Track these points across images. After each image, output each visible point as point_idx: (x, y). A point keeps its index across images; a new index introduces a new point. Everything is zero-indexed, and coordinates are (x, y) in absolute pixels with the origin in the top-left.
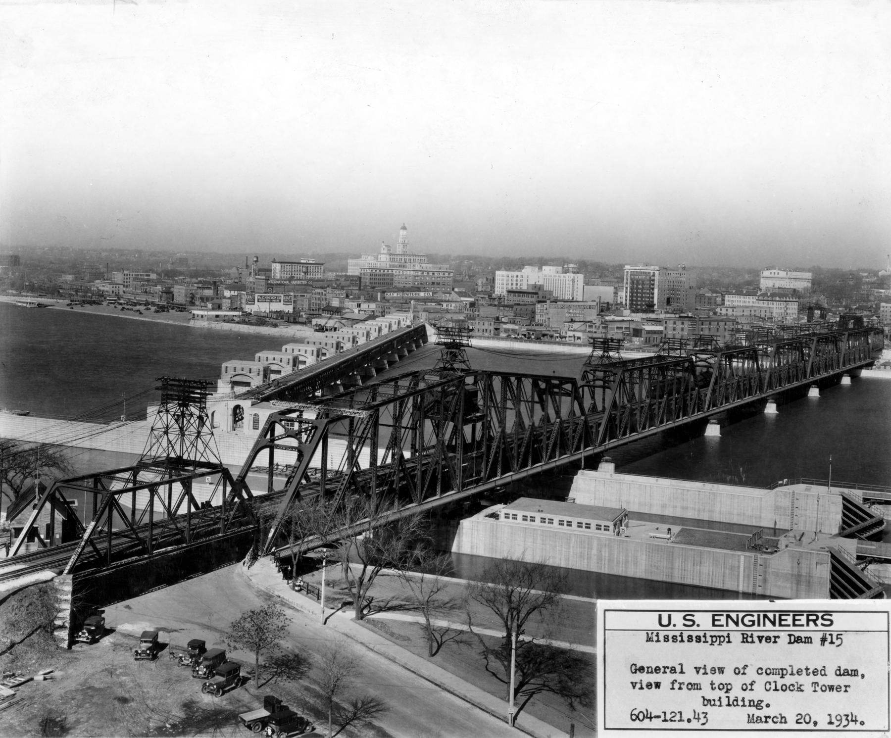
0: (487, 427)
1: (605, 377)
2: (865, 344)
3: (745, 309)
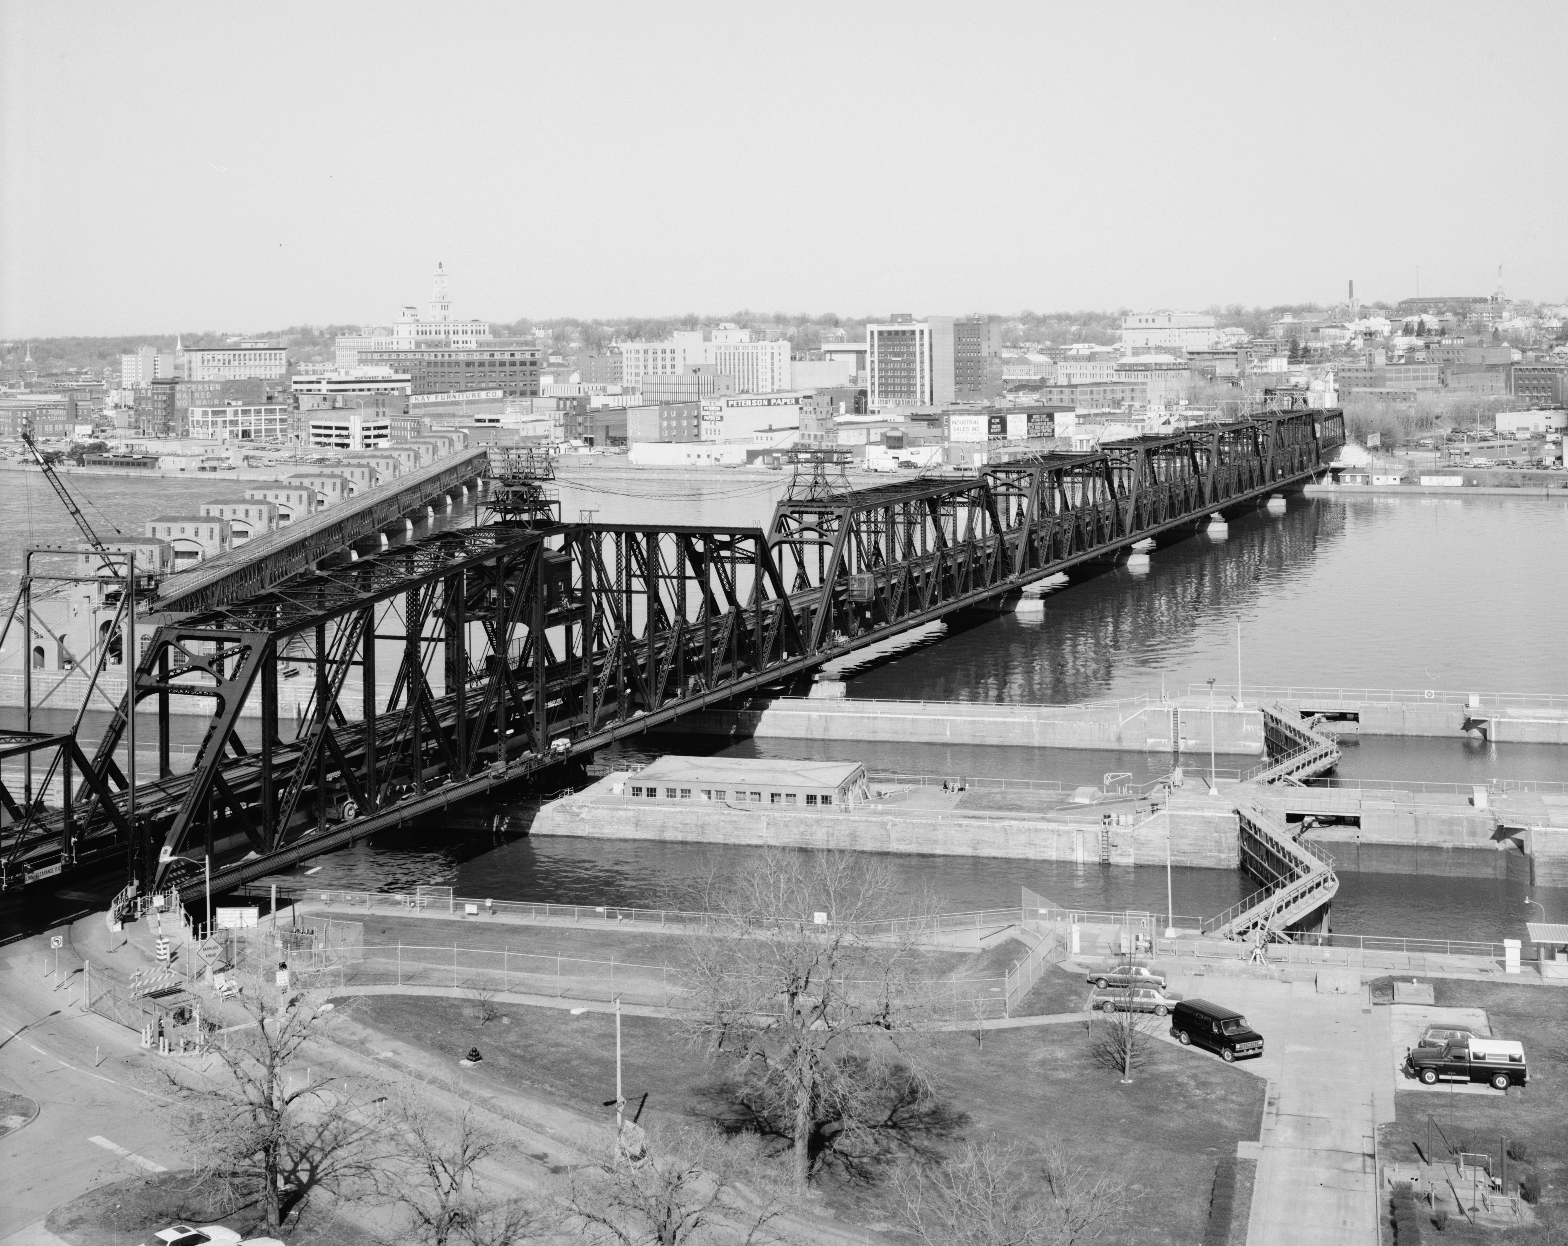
0: (593, 631)
1: (820, 525)
2: (1310, 439)
3: (1095, 389)
